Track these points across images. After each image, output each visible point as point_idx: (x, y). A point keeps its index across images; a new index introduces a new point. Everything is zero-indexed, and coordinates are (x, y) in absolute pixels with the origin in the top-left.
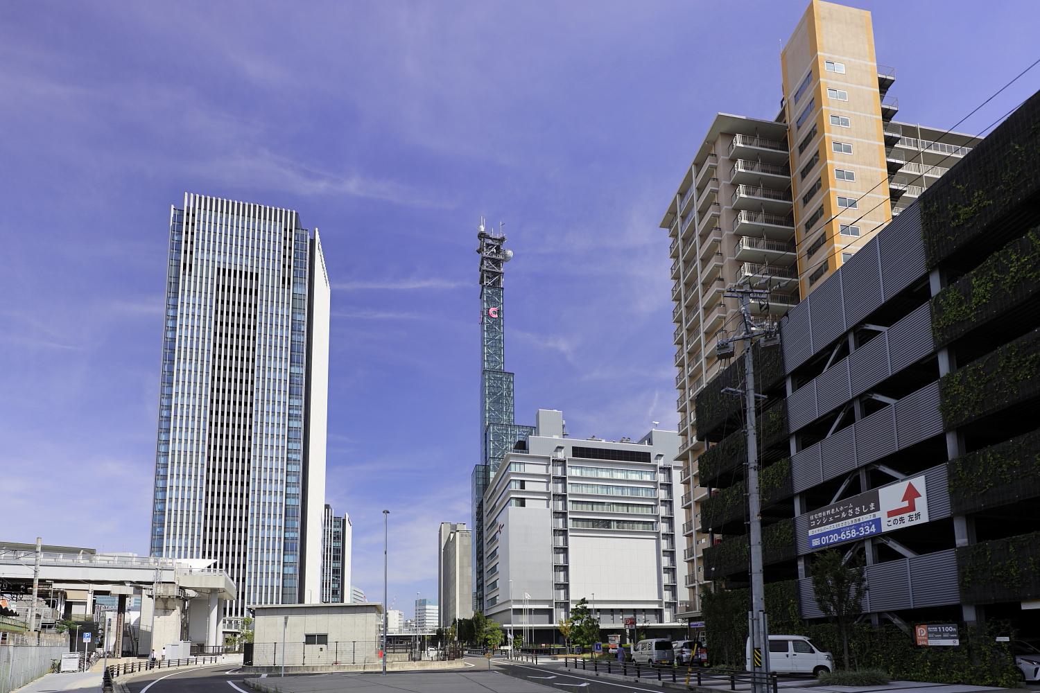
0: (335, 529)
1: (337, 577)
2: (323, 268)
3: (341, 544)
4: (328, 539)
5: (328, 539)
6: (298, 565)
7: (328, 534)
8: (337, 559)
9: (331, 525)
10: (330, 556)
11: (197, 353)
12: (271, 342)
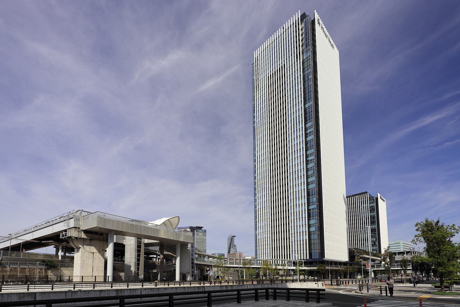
0: (371, 205)
1: (374, 234)
2: (326, 36)
3: (375, 213)
4: (366, 212)
5: (366, 212)
6: (378, 250)
7: (366, 209)
8: (374, 223)
9: (368, 203)
10: (369, 221)
11: (366, 247)
12: (296, 203)
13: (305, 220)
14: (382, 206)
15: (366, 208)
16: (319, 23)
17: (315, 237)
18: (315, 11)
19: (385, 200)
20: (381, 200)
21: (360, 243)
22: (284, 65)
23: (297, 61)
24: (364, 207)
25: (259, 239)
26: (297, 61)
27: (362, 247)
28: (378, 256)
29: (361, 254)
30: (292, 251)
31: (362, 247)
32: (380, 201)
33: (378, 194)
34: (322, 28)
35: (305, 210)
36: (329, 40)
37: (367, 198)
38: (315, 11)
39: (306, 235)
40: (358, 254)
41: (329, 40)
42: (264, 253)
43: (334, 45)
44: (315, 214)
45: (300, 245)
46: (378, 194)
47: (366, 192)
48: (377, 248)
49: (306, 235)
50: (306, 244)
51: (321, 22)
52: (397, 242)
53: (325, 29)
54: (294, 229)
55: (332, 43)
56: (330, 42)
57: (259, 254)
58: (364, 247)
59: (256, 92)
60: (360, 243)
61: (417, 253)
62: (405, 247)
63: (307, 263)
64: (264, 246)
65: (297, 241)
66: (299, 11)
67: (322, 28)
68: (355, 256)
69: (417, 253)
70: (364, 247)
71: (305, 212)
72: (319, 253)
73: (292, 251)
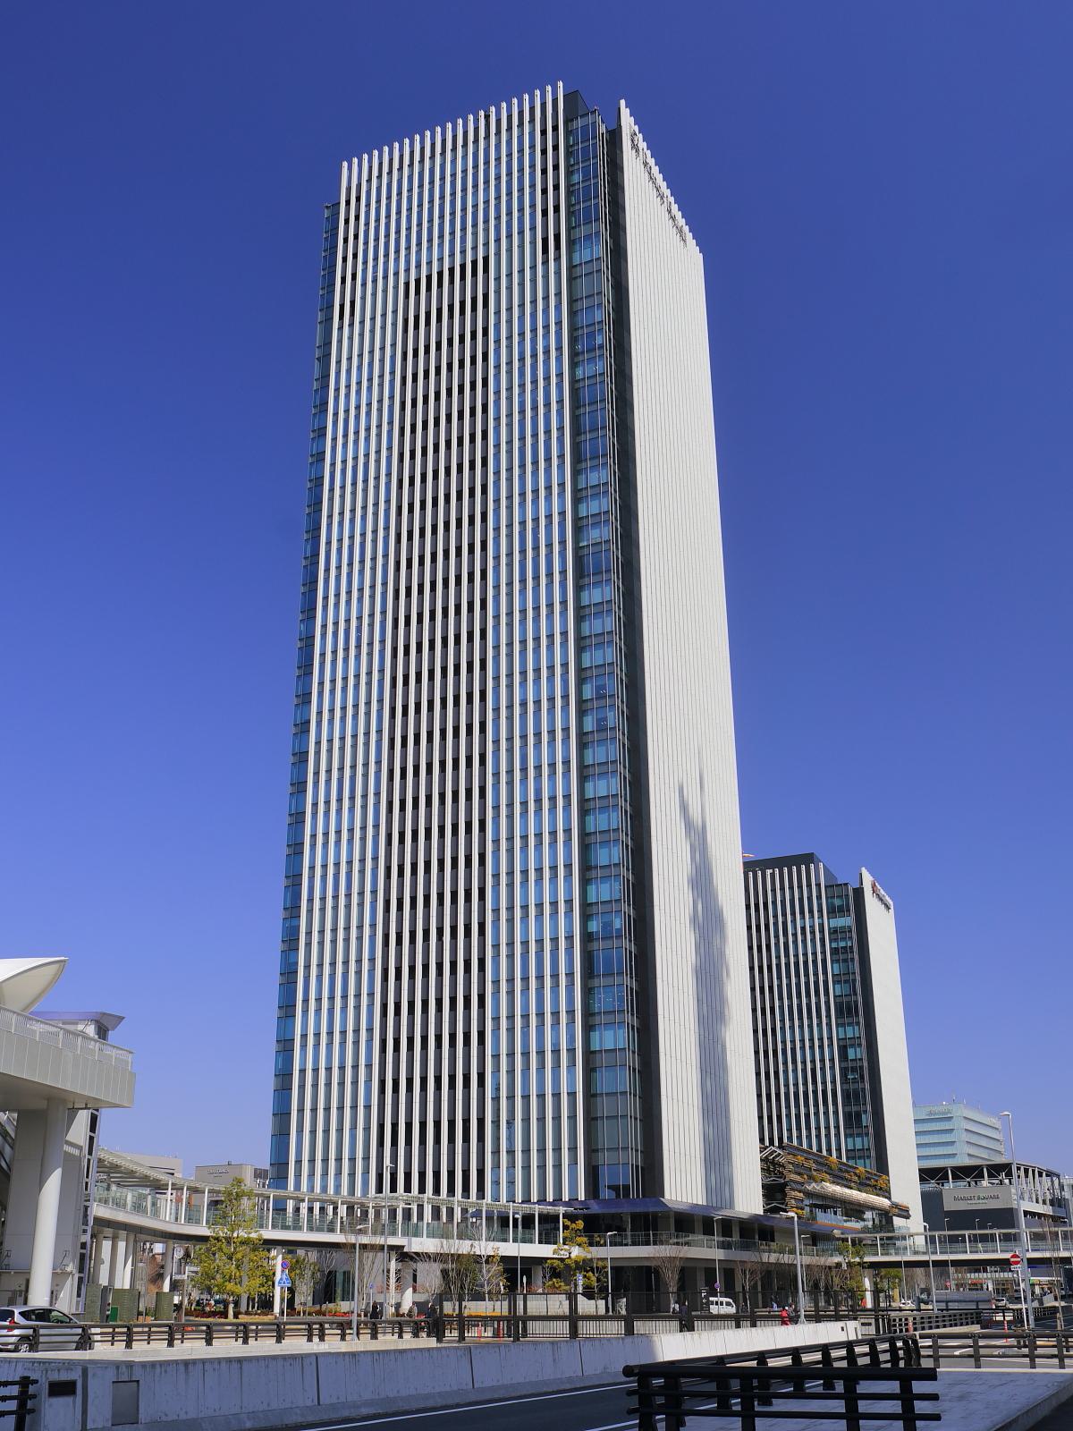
9: (820, 911)
13: (570, 985)
14: (881, 926)
15: (813, 932)
16: (635, 147)
17: (622, 1080)
18: (623, 103)
19: (892, 907)
20: (875, 900)
21: (789, 1116)
22: (486, 259)
23: (545, 262)
24: (803, 929)
25: (303, 1071)
26: (545, 262)
27: (799, 1137)
28: (875, 1186)
29: (811, 1178)
30: (496, 1152)
31: (799, 1137)
32: (872, 905)
33: (864, 871)
34: (645, 164)
35: (570, 938)
36: (670, 212)
37: (818, 885)
38: (623, 103)
39: (572, 1064)
40: (798, 1178)
41: (670, 212)
42: (332, 1156)
43: (686, 229)
44: (620, 962)
45: (557, 1118)
46: (864, 871)
47: (808, 859)
48: (869, 1142)
49: (572, 1064)
50: (573, 1117)
51: (643, 145)
52: (940, 1109)
53: (655, 170)
54: (358, 1008)
55: (681, 222)
56: (673, 218)
57: (299, 1162)
58: (809, 1137)
59: (341, 328)
60: (789, 1116)
61: (1033, 1171)
62: (974, 1139)
63: (594, 1227)
64: (334, 1112)
65: (526, 1098)
66: (560, 84)
67: (645, 164)
68: (785, 1184)
69: (1033, 1171)
70: (809, 1137)
71: (570, 949)
72: (637, 1167)
73: (496, 1152)
